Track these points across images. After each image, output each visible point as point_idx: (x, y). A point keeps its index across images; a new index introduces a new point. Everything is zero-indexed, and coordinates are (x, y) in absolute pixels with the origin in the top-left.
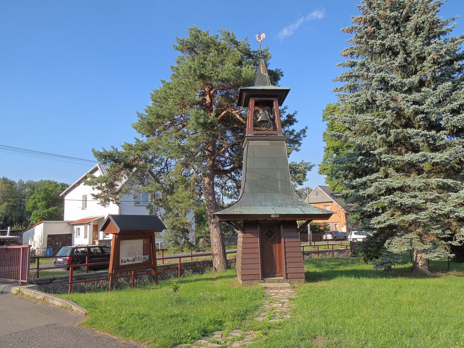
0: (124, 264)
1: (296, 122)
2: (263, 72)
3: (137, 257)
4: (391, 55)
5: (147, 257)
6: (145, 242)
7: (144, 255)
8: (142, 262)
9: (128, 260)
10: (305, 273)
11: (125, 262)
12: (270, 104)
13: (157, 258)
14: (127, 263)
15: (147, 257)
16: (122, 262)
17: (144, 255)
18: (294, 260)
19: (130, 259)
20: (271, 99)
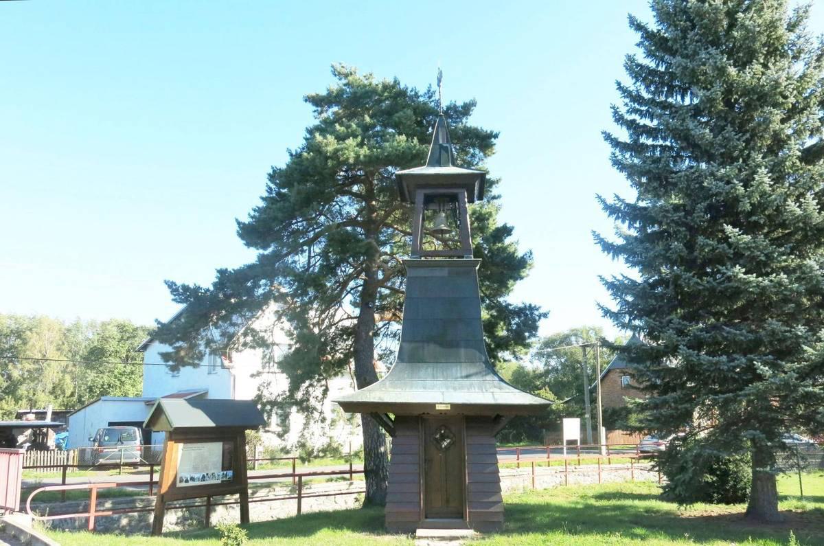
0: (184, 485)
1: (496, 136)
2: (443, 141)
3: (210, 474)
4: (548, 384)
5: (230, 473)
6: (227, 446)
7: (222, 470)
8: (219, 481)
9: (192, 479)
10: (649, 70)
11: (187, 481)
12: (454, 198)
13: (363, 474)
14: (191, 484)
15: (230, 473)
16: (181, 481)
17: (222, 470)
18: (55, 461)
19: (196, 476)
20: (455, 191)
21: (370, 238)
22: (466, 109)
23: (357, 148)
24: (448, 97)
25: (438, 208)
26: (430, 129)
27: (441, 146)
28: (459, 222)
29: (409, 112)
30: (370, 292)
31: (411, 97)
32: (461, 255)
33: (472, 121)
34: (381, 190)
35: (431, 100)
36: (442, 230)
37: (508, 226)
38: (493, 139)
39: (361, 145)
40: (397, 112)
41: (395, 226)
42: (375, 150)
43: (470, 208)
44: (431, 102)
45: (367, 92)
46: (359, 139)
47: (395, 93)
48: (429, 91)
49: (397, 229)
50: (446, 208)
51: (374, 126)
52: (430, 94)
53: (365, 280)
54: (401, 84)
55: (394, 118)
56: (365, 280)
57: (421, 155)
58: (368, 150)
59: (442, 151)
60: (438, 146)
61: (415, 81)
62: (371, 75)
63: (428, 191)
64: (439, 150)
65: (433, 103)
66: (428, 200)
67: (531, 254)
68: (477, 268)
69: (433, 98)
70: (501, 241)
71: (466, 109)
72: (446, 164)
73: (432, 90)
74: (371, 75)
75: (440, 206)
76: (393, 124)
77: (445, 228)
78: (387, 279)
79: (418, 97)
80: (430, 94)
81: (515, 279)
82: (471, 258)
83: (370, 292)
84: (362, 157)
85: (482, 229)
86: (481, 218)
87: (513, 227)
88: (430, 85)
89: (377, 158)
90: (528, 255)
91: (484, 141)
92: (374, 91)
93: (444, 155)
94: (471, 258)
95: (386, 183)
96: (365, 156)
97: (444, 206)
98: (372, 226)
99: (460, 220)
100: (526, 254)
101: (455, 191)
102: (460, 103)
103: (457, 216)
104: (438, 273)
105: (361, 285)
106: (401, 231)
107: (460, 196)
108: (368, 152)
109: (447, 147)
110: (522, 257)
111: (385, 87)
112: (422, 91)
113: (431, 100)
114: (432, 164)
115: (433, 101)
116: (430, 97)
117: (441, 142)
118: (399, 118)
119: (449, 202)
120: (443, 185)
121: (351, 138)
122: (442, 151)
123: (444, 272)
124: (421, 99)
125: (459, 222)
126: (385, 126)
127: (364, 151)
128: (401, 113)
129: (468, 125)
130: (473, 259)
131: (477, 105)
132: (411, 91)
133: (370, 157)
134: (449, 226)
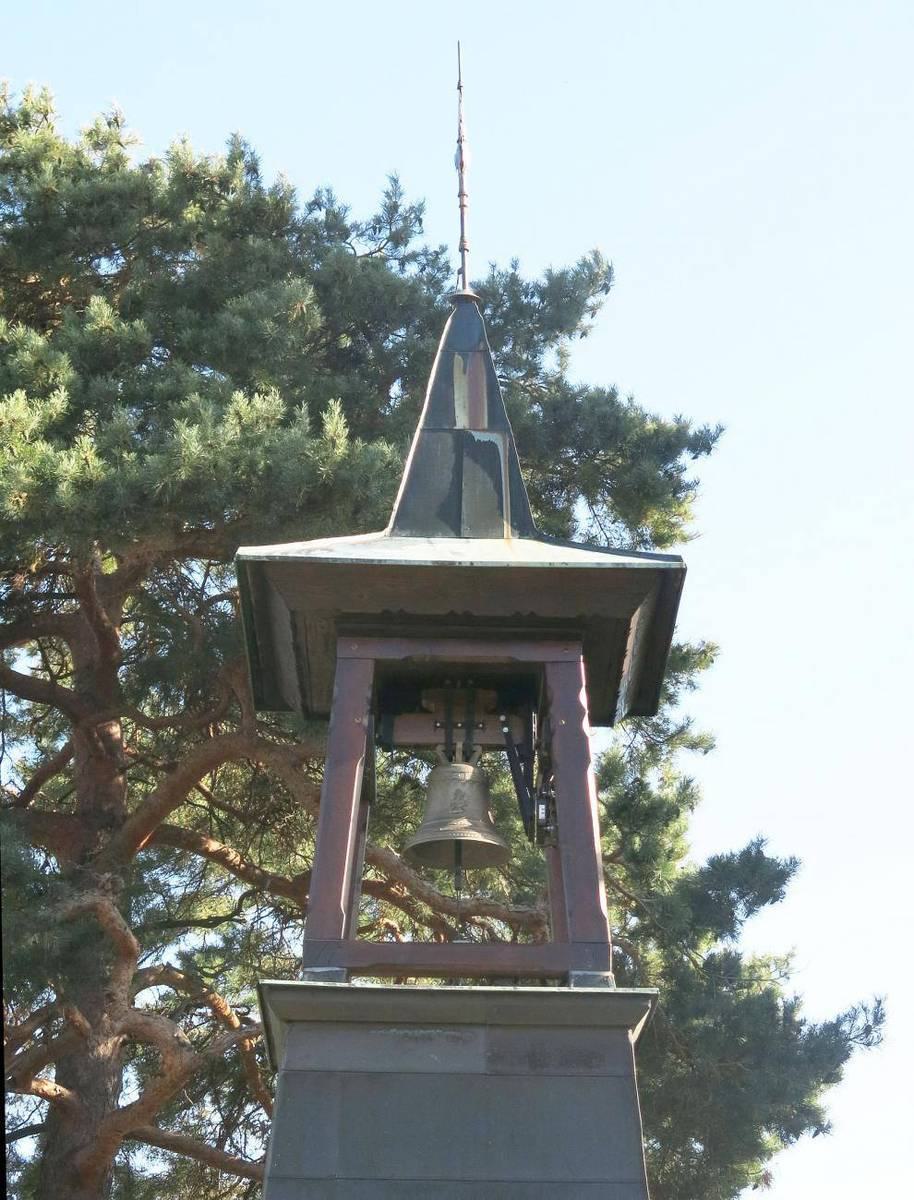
1: (702, 444)
12: (520, 692)
20: (526, 654)
21: (94, 884)
22: (564, 303)
23: (43, 447)
24: (492, 239)
25: (439, 737)
26: (395, 390)
27: (463, 439)
28: (542, 811)
29: (303, 297)
30: (80, 1159)
31: (309, 231)
32: (557, 968)
33: (584, 362)
34: (151, 672)
35: (403, 251)
36: (459, 845)
37: (769, 852)
38: (685, 458)
39: (61, 432)
40: (239, 293)
41: (214, 846)
42: (130, 457)
43: (602, 742)
44: (403, 262)
45: (101, 198)
46: (59, 401)
47: (235, 210)
48: (392, 209)
49: (220, 857)
50: (479, 737)
51: (138, 352)
52: (398, 222)
53: (56, 1103)
54: (262, 169)
55: (224, 317)
56: (56, 1103)
57: (357, 491)
58: (99, 455)
59: (467, 462)
60: (449, 440)
61: (325, 161)
62: (114, 122)
63: (395, 651)
64: (451, 458)
65: (412, 269)
66: (397, 697)
67: (879, 1018)
68: (633, 1036)
69: (415, 244)
70: (725, 925)
71: (564, 303)
72: (486, 528)
73: (405, 204)
74: (114, 122)
75: (449, 727)
76: (222, 344)
77: (476, 836)
78: (164, 1099)
79: (345, 233)
80: (398, 222)
81: (791, 1130)
82: (605, 982)
83: (80, 1159)
84: (64, 488)
85: (641, 862)
86: (643, 816)
87: (794, 863)
88: (395, 181)
89: (141, 495)
90: (860, 1022)
91: (639, 463)
92: (135, 194)
93: (475, 482)
94: (605, 982)
95: (371, 328)
96: (82, 485)
97: (470, 727)
98: (103, 838)
99: (550, 801)
100: (852, 1017)
101: (526, 654)
102: (532, 274)
103: (545, 765)
104: (435, 1055)
105: (31, 1130)
106: (244, 874)
107: (554, 682)
108: (96, 463)
109: (492, 445)
110: (833, 1029)
111: (190, 183)
112: (362, 207)
113: (403, 251)
114: (413, 523)
115: (413, 257)
116: (399, 239)
117: (462, 421)
118: (246, 315)
119: (496, 712)
120: (468, 619)
121: (20, 394)
122: (467, 462)
123: (469, 1055)
124: (360, 247)
125: (542, 811)
126: (189, 354)
127: (80, 460)
128: (261, 296)
129: (575, 379)
130: (613, 989)
131: (617, 285)
132: (316, 204)
133: (106, 489)
134: (493, 829)
